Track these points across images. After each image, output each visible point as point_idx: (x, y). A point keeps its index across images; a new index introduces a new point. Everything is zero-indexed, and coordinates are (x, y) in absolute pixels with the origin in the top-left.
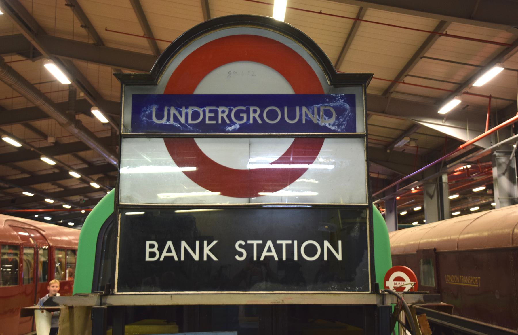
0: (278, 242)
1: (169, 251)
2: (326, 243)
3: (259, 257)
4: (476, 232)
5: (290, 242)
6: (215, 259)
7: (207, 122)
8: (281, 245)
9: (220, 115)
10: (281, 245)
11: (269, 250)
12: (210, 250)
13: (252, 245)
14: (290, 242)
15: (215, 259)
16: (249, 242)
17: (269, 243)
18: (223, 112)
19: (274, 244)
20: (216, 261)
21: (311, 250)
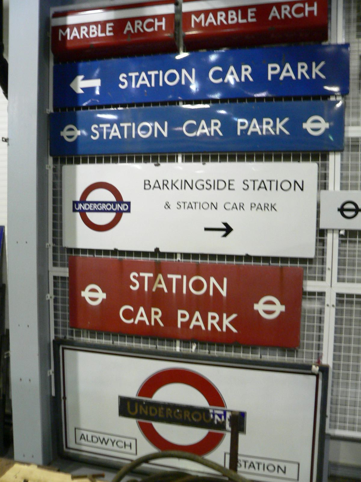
0: (169, 276)
1: (197, 320)
2: (212, 280)
5: (179, 277)
6: (234, 330)
10: (172, 279)
12: (231, 323)
14: (179, 277)
15: (234, 330)
16: (142, 274)
20: (235, 333)
21: (198, 285)
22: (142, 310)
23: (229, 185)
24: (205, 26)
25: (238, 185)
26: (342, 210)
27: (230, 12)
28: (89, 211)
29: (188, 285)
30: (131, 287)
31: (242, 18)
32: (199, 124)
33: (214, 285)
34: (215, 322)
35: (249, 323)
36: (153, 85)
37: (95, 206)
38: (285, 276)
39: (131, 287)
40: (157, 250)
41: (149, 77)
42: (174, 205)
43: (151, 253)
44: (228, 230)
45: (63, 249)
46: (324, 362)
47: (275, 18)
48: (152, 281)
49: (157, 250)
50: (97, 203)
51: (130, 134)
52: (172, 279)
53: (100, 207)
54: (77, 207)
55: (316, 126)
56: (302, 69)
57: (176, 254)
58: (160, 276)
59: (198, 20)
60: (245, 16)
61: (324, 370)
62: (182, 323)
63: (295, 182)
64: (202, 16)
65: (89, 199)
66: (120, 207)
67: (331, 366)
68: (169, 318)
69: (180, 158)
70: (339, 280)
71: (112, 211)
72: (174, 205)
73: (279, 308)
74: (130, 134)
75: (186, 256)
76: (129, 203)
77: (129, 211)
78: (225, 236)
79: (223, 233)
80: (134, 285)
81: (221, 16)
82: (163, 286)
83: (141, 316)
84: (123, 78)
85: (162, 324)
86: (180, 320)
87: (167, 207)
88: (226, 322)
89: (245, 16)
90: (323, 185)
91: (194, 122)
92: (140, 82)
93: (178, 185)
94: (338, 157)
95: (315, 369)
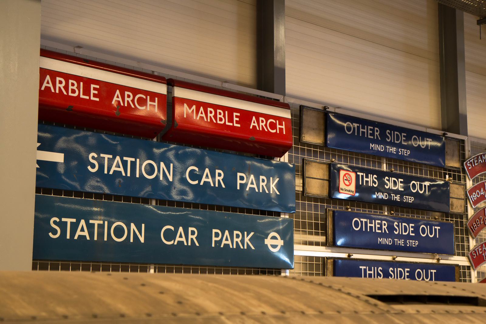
0: (125, 158)
2: (133, 226)
3: (109, 170)
4: (263, 160)
5: (133, 160)
8: (94, 224)
11: (82, 230)
14: (133, 160)
16: (64, 220)
22: (181, 229)
34: (239, 240)
36: (129, 175)
41: (125, 163)
51: (101, 234)
60: (87, 91)
62: (215, 241)
74: (101, 234)
88: (247, 240)
89: (87, 91)
91: (172, 228)
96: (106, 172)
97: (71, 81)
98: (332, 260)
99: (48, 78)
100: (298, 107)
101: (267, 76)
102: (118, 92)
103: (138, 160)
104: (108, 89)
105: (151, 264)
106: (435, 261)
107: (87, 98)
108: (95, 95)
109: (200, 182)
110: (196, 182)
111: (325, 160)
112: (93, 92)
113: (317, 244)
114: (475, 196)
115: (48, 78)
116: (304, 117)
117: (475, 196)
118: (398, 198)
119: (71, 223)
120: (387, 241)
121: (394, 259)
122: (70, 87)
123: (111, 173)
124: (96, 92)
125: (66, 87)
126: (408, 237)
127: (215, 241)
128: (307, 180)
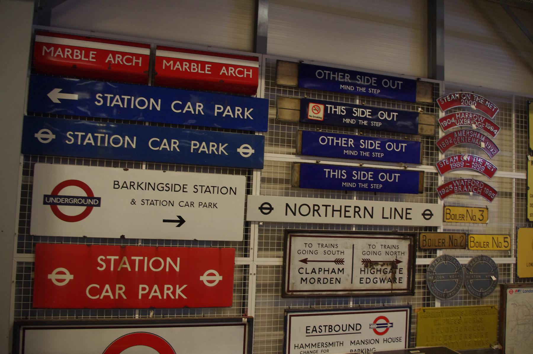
0: (123, 97)
2: (169, 259)
7: (369, 179)
9: (350, 143)
10: (135, 260)
11: (89, 139)
12: (181, 291)
13: (110, 260)
14: (142, 258)
16: (108, 257)
17: (90, 135)
18: (120, 289)
19: (93, 136)
21: (157, 264)
23: (184, 188)
24: (173, 70)
25: (190, 189)
26: (261, 208)
27: (75, 50)
28: (61, 204)
29: (148, 264)
30: (99, 268)
31: (85, 58)
32: (162, 141)
33: (170, 263)
35: (196, 290)
36: (125, 106)
37: (67, 200)
38: (220, 254)
39: (99, 268)
40: (123, 237)
41: (123, 100)
42: (139, 202)
43: (117, 239)
44: (181, 221)
45: (30, 237)
46: (249, 315)
47: (224, 74)
48: (117, 263)
49: (123, 237)
50: (69, 197)
52: (135, 260)
53: (71, 201)
54: (48, 200)
55: (246, 151)
56: (238, 111)
57: (138, 239)
58: (125, 258)
59: (168, 65)
60: (203, 69)
61: (250, 320)
63: (231, 188)
64: (172, 62)
65: (60, 194)
66: (90, 201)
67: (254, 317)
68: (131, 292)
69: (144, 166)
70: (258, 256)
71: (83, 205)
72: (139, 202)
73: (218, 278)
75: (146, 241)
76: (99, 199)
77: (99, 205)
78: (179, 226)
79: (178, 224)
80: (101, 266)
81: (68, 51)
82: (128, 266)
83: (107, 291)
84: (99, 97)
85: (125, 297)
86: (141, 292)
87: (133, 203)
89: (203, 69)
90: (249, 192)
92: (114, 102)
93: (143, 186)
94: (259, 173)
95: (245, 320)
96: (108, 105)
97: (192, 64)
98: (299, 164)
99: (178, 63)
100: (276, 62)
101: (258, 42)
102: (224, 68)
103: (133, 98)
104: (216, 67)
105: (142, 161)
106: (402, 168)
107: (203, 72)
108: (208, 71)
109: (182, 111)
110: (180, 111)
111: (299, 97)
112: (207, 69)
113: (290, 154)
114: (446, 123)
115: (178, 63)
116: (279, 68)
117: (446, 123)
118: (365, 123)
119: (82, 135)
120: (354, 153)
121: (361, 165)
122: (192, 67)
123: (112, 105)
124: (94, 56)
125: (72, 54)
126: (374, 150)
127: (194, 149)
128: (279, 110)
